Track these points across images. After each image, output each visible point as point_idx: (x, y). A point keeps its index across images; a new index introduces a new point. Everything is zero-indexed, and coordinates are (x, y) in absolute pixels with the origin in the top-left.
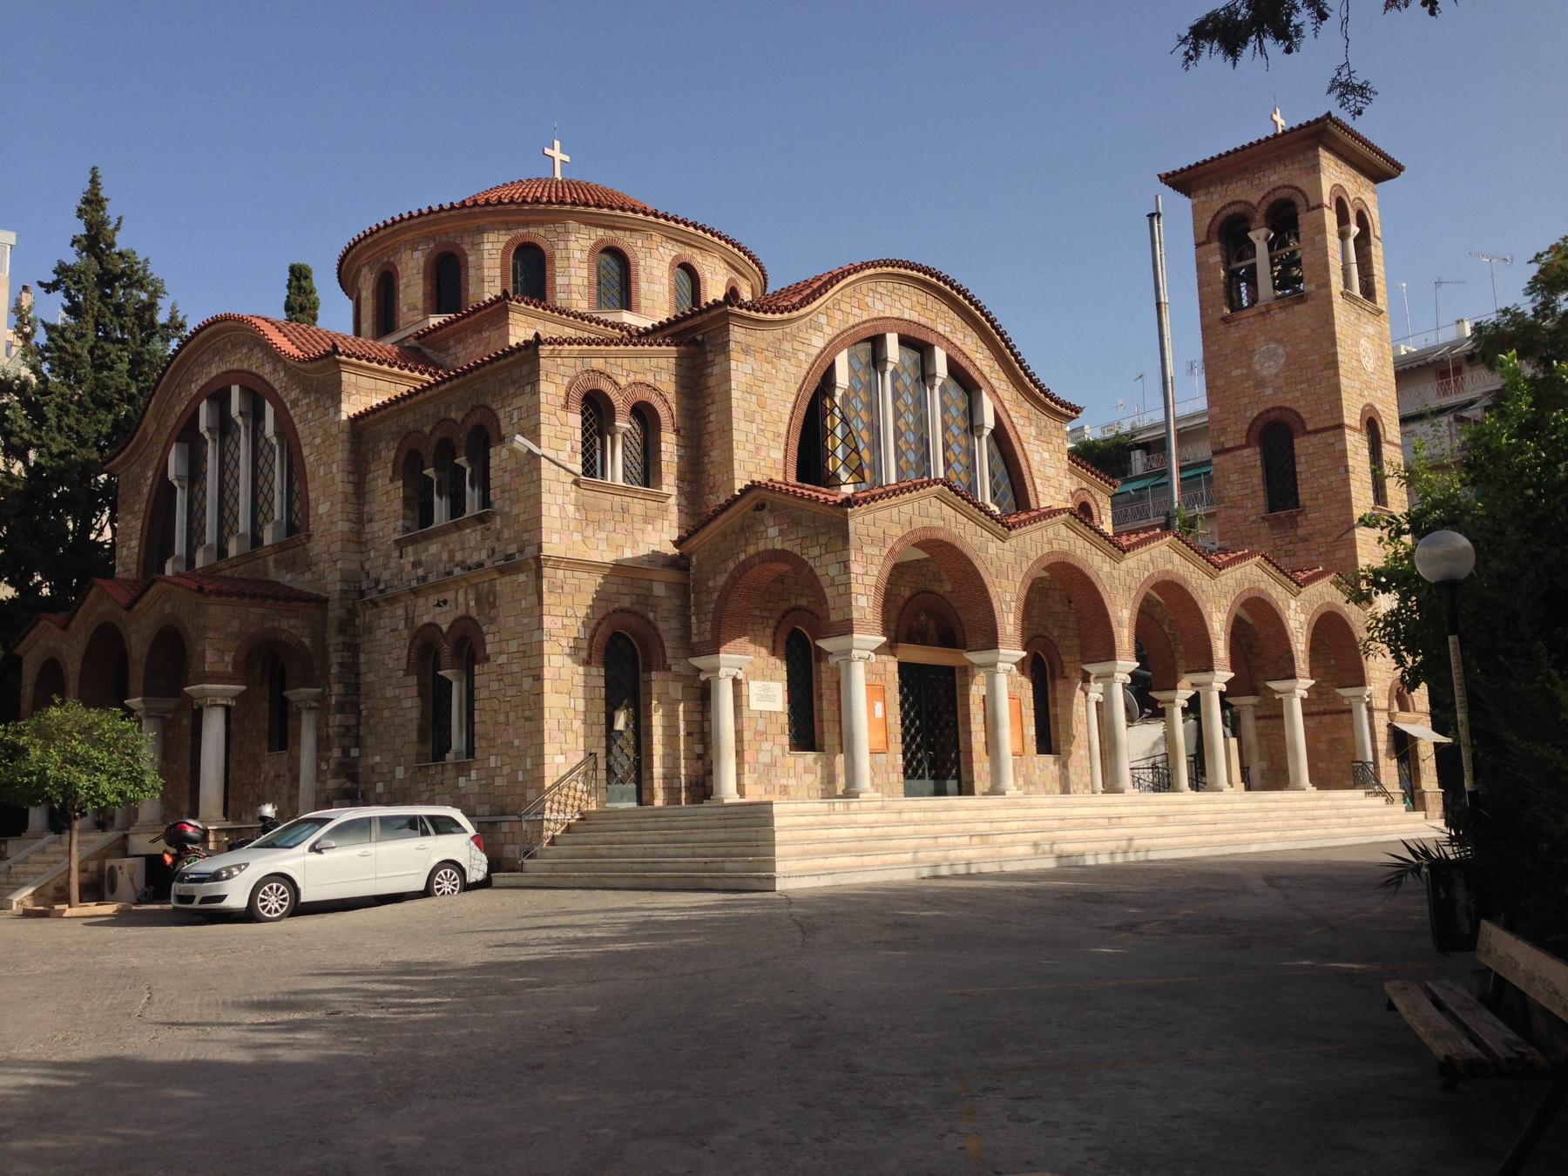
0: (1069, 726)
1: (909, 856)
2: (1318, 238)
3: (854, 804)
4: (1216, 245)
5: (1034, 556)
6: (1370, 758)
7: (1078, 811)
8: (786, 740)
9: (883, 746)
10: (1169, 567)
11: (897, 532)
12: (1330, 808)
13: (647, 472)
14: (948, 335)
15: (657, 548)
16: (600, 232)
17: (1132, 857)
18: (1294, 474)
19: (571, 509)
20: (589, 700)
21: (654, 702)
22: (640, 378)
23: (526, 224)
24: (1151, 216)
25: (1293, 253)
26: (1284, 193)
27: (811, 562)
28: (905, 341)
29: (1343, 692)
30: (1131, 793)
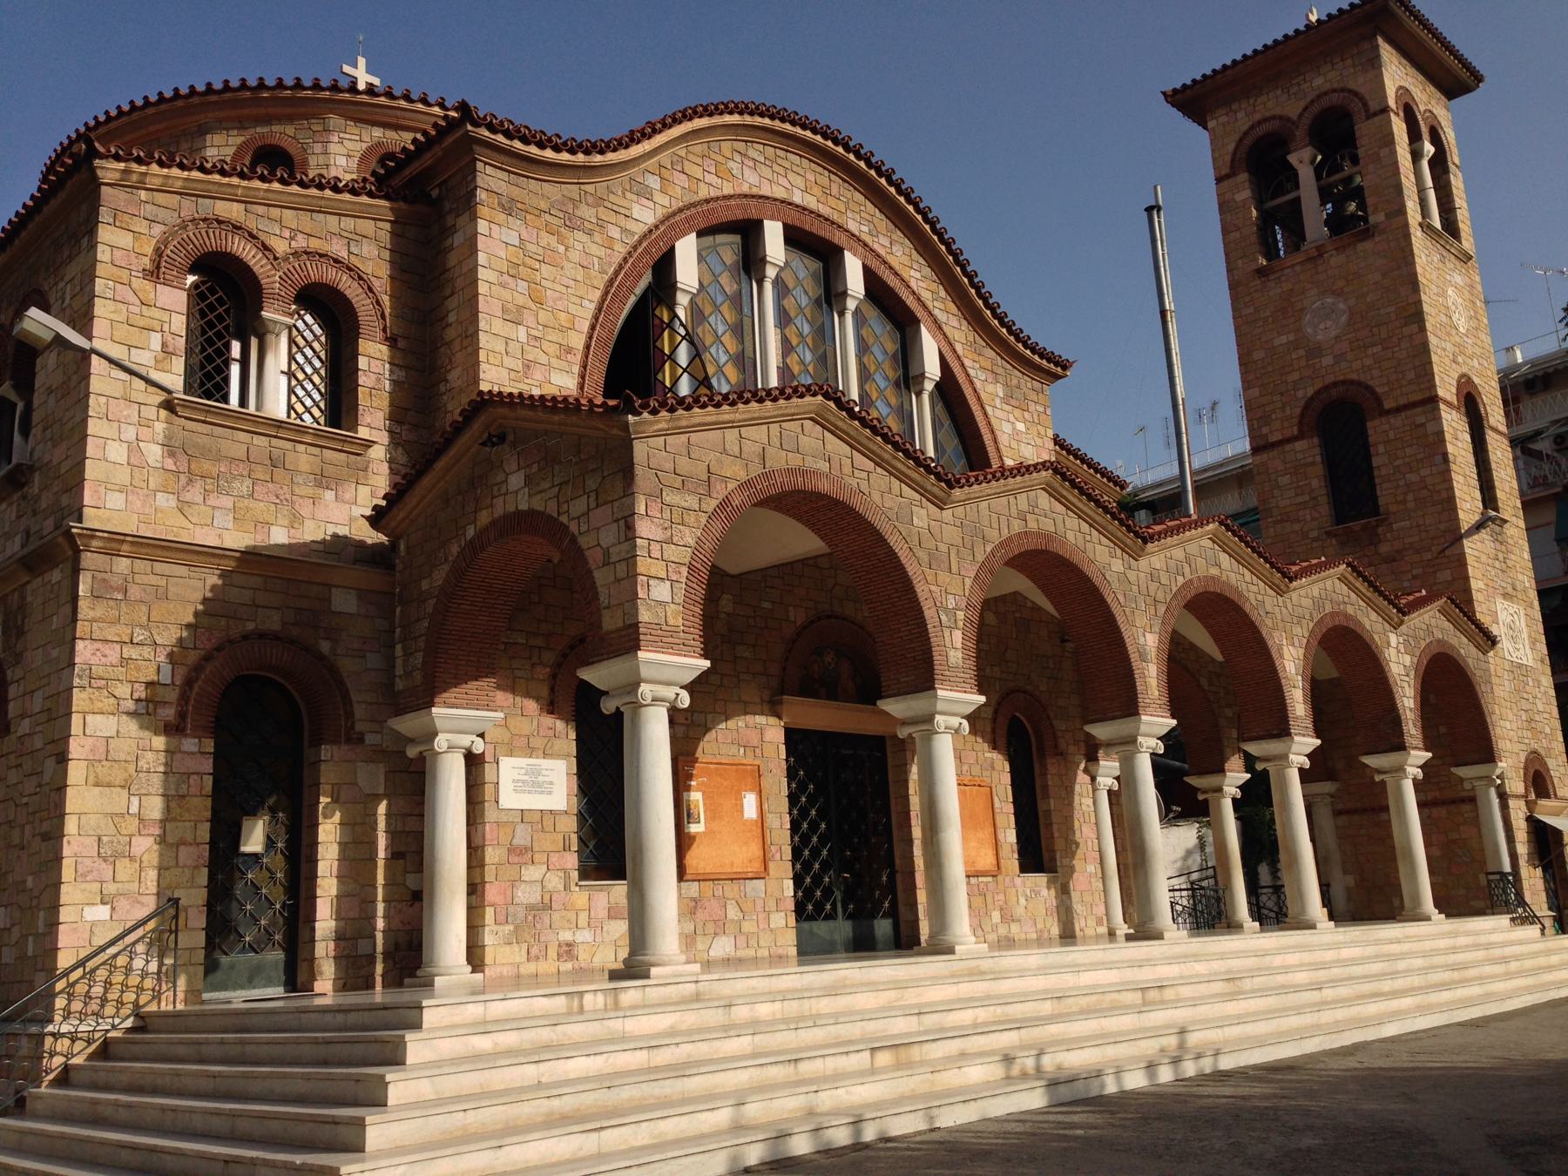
0: (1070, 828)
1: (722, 1117)
2: (1384, 152)
3: (631, 992)
4: (1243, 177)
5: (995, 537)
6: (1507, 868)
7: (1086, 978)
8: (572, 861)
9: (757, 866)
10: (1214, 571)
11: (737, 472)
12: (1476, 947)
13: (340, 403)
14: (868, 239)
15: (343, 531)
16: (377, 133)
17: (1189, 1069)
18: (1370, 468)
19: (154, 453)
20: (173, 799)
21: (324, 800)
22: (315, 244)
23: (268, 120)
24: (1149, 210)
25: (1350, 178)
26: (1335, 99)
27: (573, 527)
28: (795, 238)
29: (1463, 772)
30: (1177, 937)
